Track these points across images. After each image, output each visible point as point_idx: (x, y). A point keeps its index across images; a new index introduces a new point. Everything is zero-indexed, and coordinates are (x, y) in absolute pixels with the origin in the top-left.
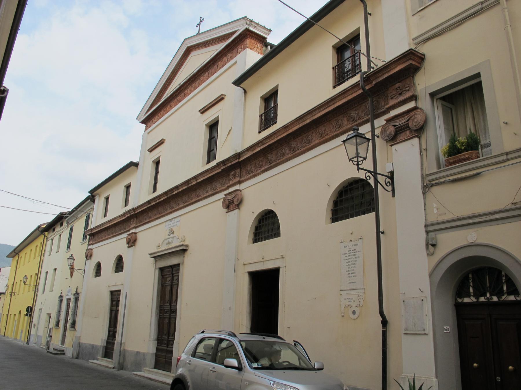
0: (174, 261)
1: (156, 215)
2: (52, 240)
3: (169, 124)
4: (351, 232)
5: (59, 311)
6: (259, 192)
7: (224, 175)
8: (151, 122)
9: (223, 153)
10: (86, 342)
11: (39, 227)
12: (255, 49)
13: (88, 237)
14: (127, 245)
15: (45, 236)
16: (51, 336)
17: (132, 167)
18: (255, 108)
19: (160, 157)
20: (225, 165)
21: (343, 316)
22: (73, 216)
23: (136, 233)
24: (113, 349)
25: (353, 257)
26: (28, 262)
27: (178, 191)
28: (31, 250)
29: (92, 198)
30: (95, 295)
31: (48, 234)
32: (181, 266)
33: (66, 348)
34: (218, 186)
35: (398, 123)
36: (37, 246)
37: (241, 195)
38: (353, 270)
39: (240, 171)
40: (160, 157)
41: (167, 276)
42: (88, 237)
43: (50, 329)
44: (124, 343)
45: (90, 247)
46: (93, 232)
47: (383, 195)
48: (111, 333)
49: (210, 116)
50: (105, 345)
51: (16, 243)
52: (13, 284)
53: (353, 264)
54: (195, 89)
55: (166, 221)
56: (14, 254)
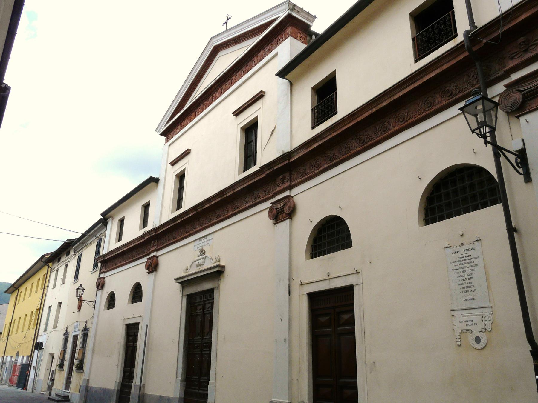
0: (207, 286)
1: (181, 235)
2: (57, 271)
3: (192, 136)
4: (461, 233)
5: (64, 350)
6: (314, 200)
7: (266, 184)
8: (172, 133)
9: (266, 154)
10: (96, 386)
11: (43, 257)
12: (299, 38)
13: (99, 264)
14: (147, 271)
15: (49, 267)
16: (53, 380)
17: (152, 183)
18: (305, 100)
19: (185, 169)
20: (271, 168)
21: (459, 346)
22: (82, 242)
23: (157, 257)
24: (129, 394)
25: (468, 265)
26: (28, 300)
27: (210, 204)
28: (33, 284)
29: (104, 221)
30: (109, 328)
31: (53, 264)
32: (215, 291)
33: (72, 394)
34: (260, 194)
35: (526, 87)
36: (39, 279)
37: (294, 202)
38: (470, 283)
39: (290, 174)
40: (185, 169)
41: (197, 304)
42: (99, 264)
43: (53, 371)
44: (144, 386)
45: (102, 276)
46: (106, 258)
47: (513, 180)
48: (127, 374)
49: (246, 117)
50: (183, 396)
51: (12, 281)
52: (11, 323)
53: (468, 275)
54: (225, 91)
55: (194, 241)
56: (13, 289)
